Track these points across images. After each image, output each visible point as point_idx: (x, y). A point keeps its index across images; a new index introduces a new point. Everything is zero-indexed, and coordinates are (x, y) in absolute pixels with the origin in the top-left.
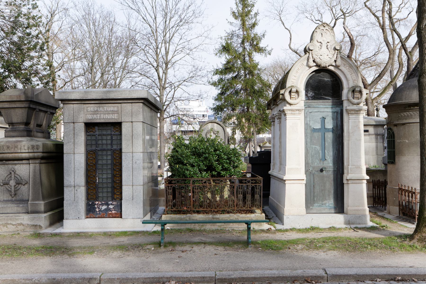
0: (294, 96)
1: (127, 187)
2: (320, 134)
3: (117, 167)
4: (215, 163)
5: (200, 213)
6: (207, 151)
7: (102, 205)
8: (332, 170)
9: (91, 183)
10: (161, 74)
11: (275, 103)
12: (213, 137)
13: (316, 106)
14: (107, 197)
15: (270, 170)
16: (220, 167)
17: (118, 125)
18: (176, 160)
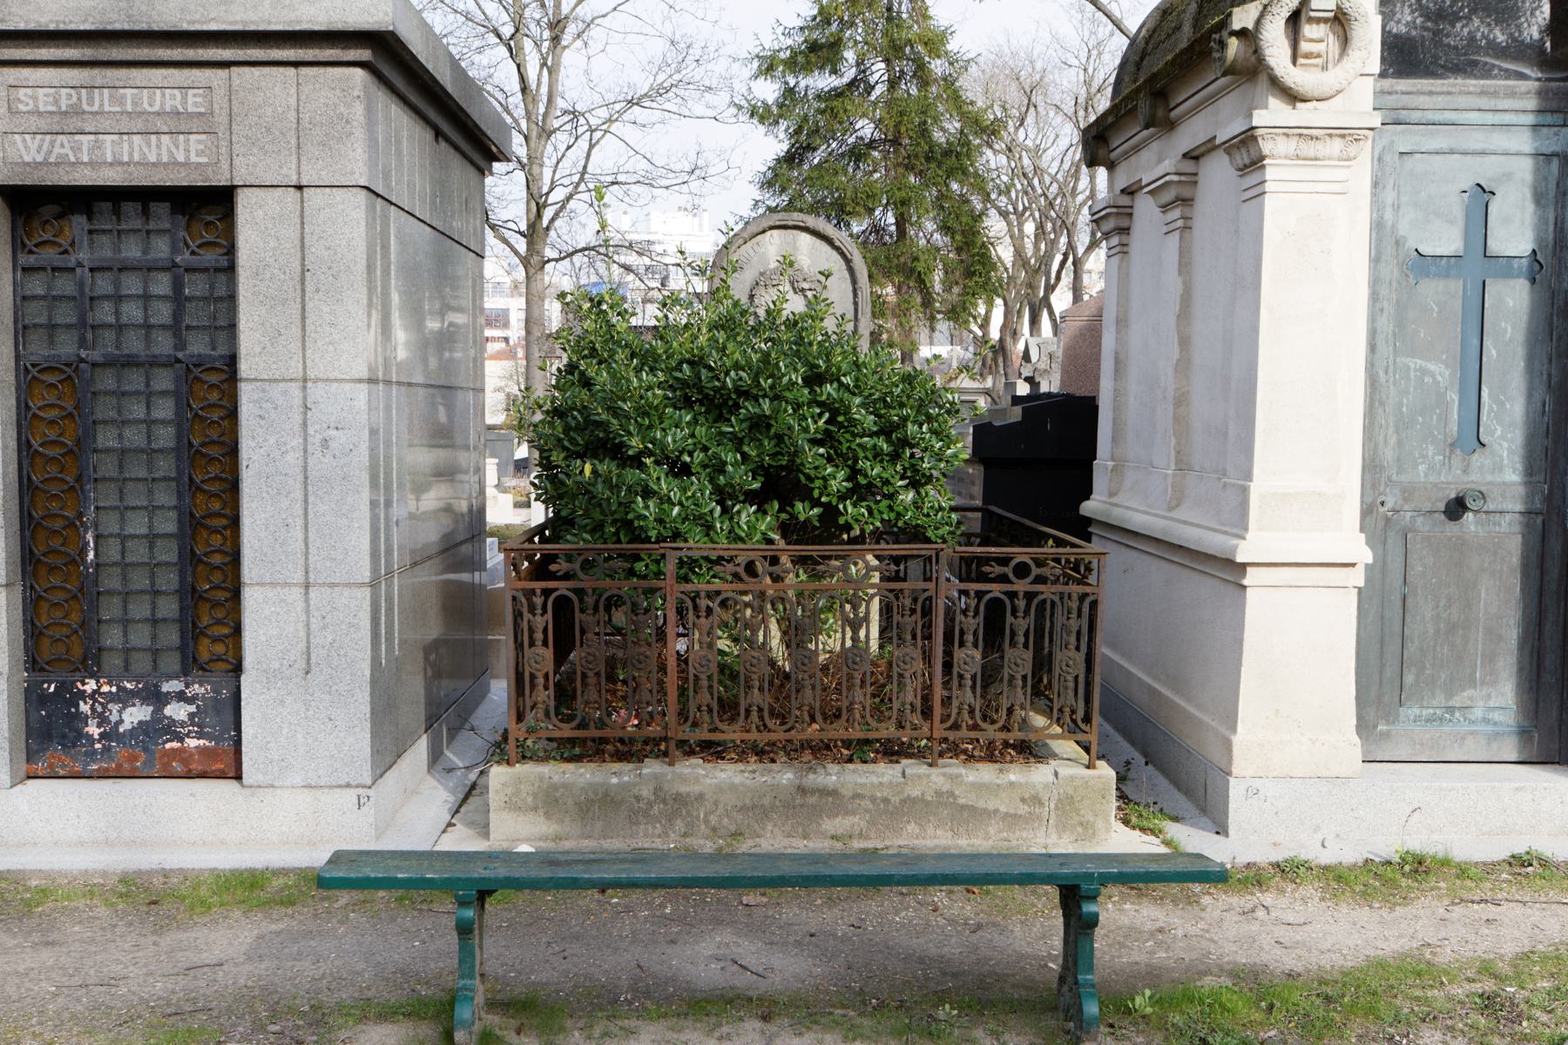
0: (1320, 47)
1: (271, 593)
2: (1456, 286)
3: (214, 470)
4: (813, 456)
5: (720, 756)
6: (766, 383)
7: (124, 698)
8: (1519, 507)
9: (53, 569)
10: (532, 72)
11: (1160, 113)
12: (795, 305)
13: (1437, 117)
14: (155, 653)
15: (1087, 493)
16: (841, 475)
17: (208, 206)
18: (579, 433)
